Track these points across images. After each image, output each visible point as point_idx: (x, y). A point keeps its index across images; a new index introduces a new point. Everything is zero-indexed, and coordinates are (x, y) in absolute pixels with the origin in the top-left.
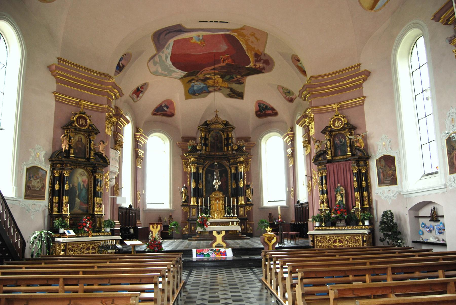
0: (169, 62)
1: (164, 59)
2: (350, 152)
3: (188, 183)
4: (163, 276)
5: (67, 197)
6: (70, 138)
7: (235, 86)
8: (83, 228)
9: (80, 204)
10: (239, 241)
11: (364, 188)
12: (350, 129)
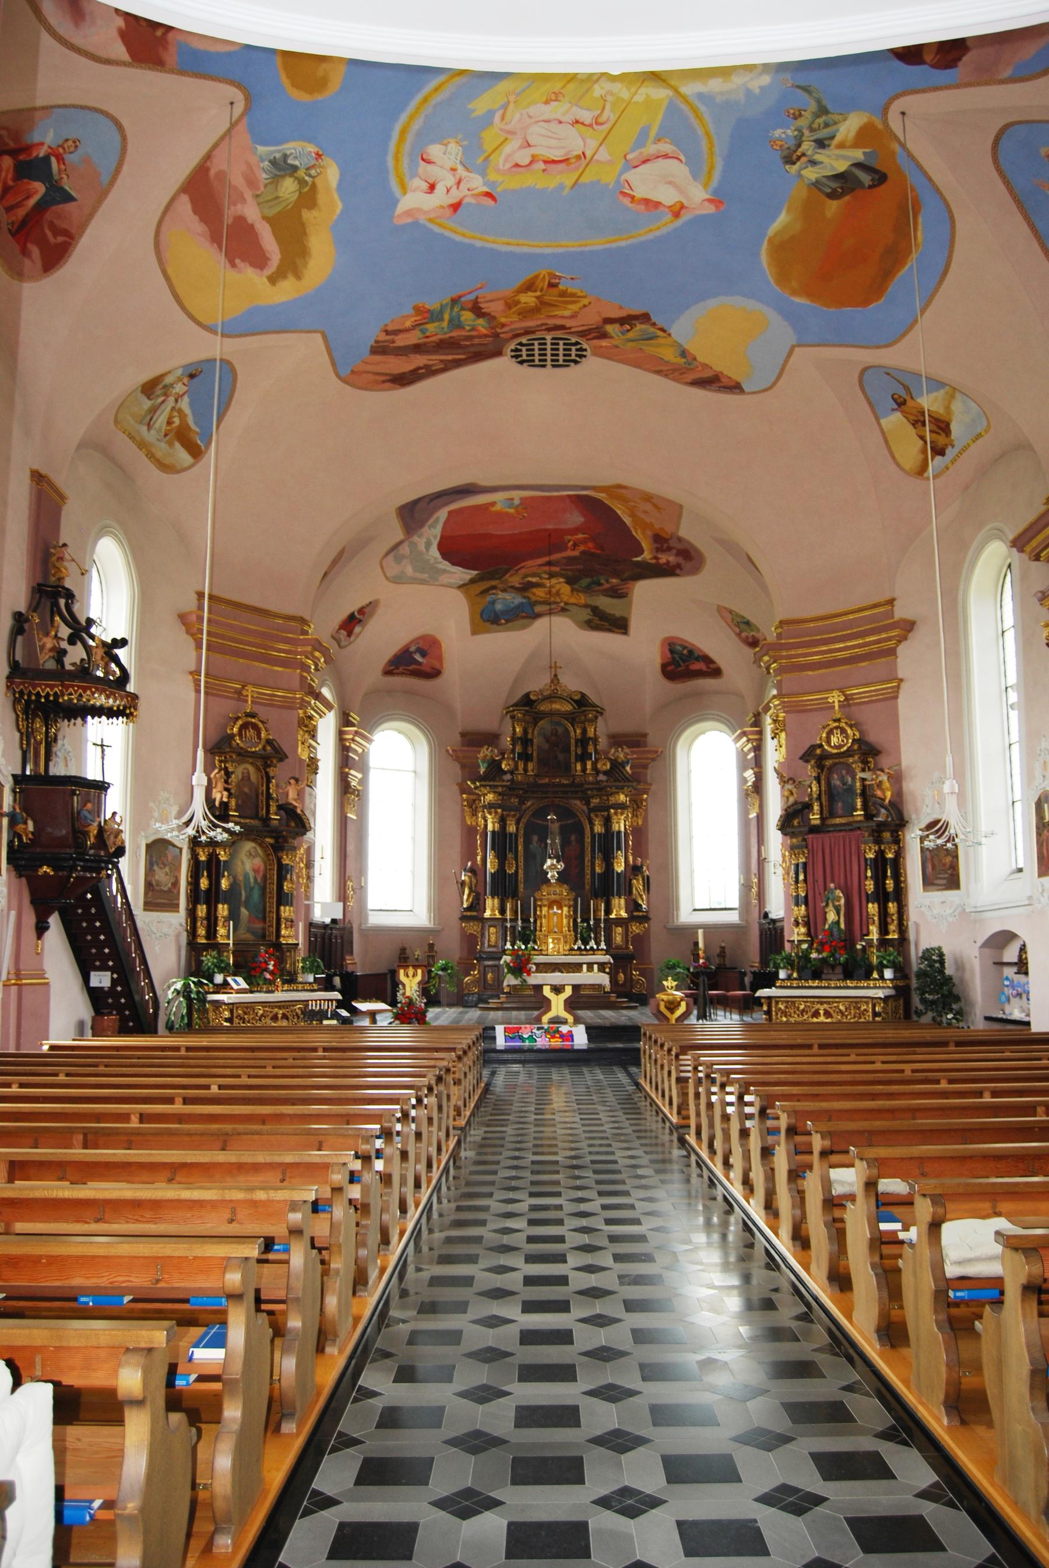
0: (435, 553)
1: (422, 547)
2: (861, 810)
3: (479, 858)
4: (387, 1134)
5: (226, 906)
6: (228, 774)
7: (604, 603)
8: (262, 973)
9: (250, 920)
10: (608, 1014)
11: (891, 895)
12: (863, 754)
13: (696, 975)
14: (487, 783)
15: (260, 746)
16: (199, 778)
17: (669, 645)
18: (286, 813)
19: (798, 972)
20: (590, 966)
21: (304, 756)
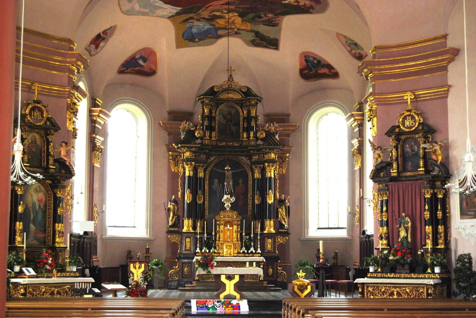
2: (423, 167)
3: (179, 194)
5: (21, 223)
7: (263, 29)
8: (44, 266)
9: (36, 233)
13: (317, 269)
14: (186, 145)
15: (43, 122)
16: (18, 146)
17: (305, 57)
18: (59, 164)
19: (381, 268)
20: (251, 264)
21: (71, 128)
